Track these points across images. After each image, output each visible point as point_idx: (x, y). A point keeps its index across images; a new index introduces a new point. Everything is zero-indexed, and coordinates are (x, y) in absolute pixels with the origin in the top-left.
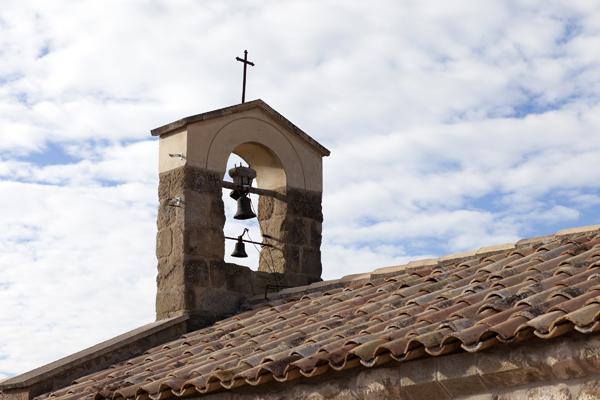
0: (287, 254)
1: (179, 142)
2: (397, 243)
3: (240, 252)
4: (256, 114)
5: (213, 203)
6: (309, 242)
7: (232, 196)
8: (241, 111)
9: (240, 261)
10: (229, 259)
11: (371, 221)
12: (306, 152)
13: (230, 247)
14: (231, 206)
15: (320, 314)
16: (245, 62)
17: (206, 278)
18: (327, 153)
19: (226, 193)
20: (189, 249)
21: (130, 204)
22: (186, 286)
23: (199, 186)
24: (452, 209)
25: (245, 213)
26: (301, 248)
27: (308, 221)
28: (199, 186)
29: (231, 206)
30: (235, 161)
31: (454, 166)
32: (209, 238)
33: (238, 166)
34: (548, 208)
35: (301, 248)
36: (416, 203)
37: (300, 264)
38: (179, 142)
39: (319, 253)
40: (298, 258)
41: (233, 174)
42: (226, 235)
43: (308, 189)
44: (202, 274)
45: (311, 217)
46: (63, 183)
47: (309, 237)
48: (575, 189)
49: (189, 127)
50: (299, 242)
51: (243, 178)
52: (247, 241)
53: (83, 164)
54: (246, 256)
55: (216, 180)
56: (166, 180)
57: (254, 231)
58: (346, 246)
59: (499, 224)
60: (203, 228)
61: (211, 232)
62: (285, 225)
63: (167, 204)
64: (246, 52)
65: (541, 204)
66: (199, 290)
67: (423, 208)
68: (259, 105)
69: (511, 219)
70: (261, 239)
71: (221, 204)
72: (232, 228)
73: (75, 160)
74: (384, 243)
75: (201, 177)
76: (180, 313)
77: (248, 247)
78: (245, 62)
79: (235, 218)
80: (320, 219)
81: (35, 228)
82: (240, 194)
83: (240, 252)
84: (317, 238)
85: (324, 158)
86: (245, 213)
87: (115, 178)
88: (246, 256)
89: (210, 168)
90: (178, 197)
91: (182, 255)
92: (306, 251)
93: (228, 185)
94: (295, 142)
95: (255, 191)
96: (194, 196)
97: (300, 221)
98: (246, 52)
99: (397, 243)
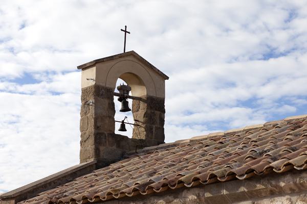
0: (147, 129)
1: (92, 73)
2: (203, 124)
3: (123, 128)
4: (131, 58)
5: (109, 104)
6: (158, 123)
7: (119, 100)
8: (124, 57)
9: (123, 133)
10: (117, 132)
11: (190, 113)
12: (156, 77)
13: (118, 126)
14: (118, 105)
15: (164, 160)
16: (126, 31)
17: (106, 142)
18: (167, 78)
19: (116, 98)
20: (96, 127)
21: (66, 104)
22: (95, 146)
23: (102, 95)
24: (231, 107)
25: (125, 109)
26: (154, 126)
27: (158, 113)
28: (102, 95)
29: (118, 105)
30: (120, 82)
31: (233, 85)
32: (107, 122)
33: (122, 84)
34: (281, 106)
35: (154, 126)
36: (213, 104)
37: (154, 134)
38: (92, 73)
39: (163, 129)
40: (152, 132)
41: (119, 89)
42: (115, 120)
43: (158, 96)
44: (104, 140)
45: (159, 111)
46: (32, 93)
47: (158, 121)
48: (294, 96)
49: (97, 65)
50: (153, 123)
51: (124, 91)
52: (126, 123)
53: (42, 84)
54: (126, 130)
55: (110, 92)
56: (85, 92)
57: (130, 118)
58: (177, 126)
59: (256, 114)
60: (104, 116)
61: (108, 118)
62: (146, 115)
63: (85, 104)
64: (126, 27)
65: (277, 104)
66: (102, 148)
67: (217, 106)
68: (132, 54)
69: (261, 112)
70: (133, 122)
71: (113, 104)
72: (119, 116)
73: (38, 82)
74: (196, 124)
75: (103, 90)
76: (92, 160)
77: (127, 126)
78: (126, 31)
79: (120, 111)
80: (164, 112)
81: (18, 116)
82: (123, 99)
83: (123, 128)
84: (162, 121)
85: (166, 81)
86: (125, 109)
87: (59, 91)
88: (126, 130)
89: (107, 86)
90: (91, 100)
91: (93, 130)
92: (157, 128)
93: (117, 95)
94: (151, 73)
95: (130, 97)
96: (99, 100)
97: (154, 113)
98: (126, 27)
99: (203, 124)
